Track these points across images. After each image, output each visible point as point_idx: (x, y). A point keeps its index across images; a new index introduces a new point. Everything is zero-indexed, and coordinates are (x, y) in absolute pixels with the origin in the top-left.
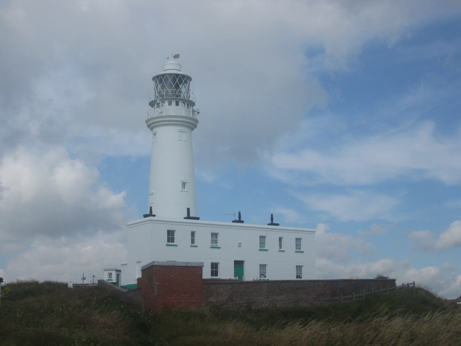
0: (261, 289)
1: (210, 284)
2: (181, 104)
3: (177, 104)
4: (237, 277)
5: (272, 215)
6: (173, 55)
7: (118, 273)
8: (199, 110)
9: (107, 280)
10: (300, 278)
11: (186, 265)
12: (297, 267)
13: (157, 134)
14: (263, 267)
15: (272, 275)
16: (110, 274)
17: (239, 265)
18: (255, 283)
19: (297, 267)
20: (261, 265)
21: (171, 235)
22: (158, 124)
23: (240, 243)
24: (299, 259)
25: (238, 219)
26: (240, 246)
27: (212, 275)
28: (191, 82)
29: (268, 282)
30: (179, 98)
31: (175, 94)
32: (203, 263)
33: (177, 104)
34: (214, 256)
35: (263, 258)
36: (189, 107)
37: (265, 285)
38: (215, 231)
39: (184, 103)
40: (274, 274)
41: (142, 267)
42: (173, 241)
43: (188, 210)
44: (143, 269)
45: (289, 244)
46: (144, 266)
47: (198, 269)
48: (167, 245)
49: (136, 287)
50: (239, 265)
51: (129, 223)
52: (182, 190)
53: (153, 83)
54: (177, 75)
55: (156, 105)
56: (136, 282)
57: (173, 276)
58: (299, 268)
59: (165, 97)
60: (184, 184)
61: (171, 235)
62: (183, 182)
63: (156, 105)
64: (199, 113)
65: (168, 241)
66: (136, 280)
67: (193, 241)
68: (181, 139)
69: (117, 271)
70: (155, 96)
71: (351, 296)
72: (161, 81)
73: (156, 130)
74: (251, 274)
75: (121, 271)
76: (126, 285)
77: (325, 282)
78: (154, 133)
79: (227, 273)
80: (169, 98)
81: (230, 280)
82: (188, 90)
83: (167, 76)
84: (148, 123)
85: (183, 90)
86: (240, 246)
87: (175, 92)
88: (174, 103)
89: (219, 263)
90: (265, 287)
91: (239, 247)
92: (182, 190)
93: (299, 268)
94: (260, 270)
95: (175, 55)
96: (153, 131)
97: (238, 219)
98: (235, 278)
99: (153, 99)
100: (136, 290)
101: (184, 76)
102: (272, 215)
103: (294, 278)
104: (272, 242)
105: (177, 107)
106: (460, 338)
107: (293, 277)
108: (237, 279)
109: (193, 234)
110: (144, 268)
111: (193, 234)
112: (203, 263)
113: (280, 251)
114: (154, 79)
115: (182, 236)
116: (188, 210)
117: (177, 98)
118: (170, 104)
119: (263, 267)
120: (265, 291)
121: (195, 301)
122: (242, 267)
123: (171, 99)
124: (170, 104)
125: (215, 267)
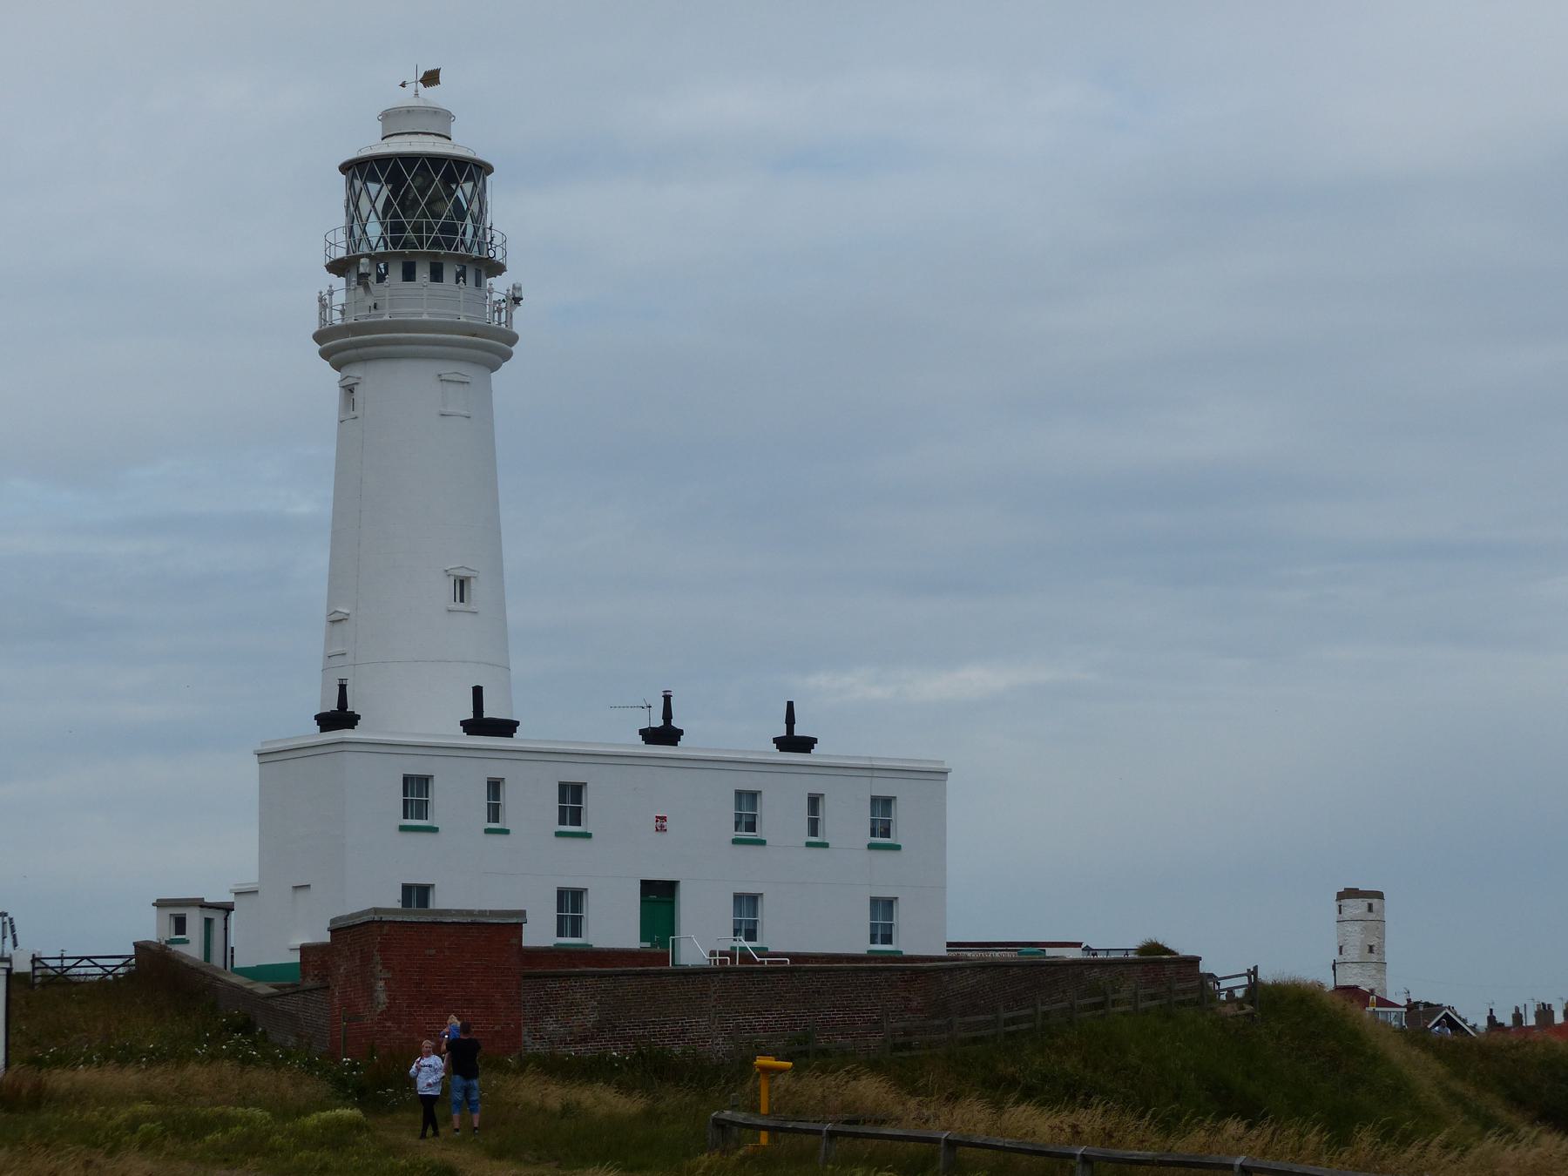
2: (449, 274)
3: (436, 275)
5: (790, 705)
6: (421, 76)
10: (887, 939)
13: (358, 390)
14: (747, 903)
15: (783, 934)
16: (180, 924)
17: (659, 898)
20: (738, 898)
21: (416, 790)
22: (360, 351)
23: (664, 819)
24: (884, 875)
27: (560, 933)
32: (522, 913)
33: (436, 275)
34: (572, 864)
35: (749, 870)
38: (748, 784)
41: (333, 921)
43: (478, 692)
45: (848, 819)
46: (340, 918)
47: (508, 928)
48: (403, 828)
50: (659, 898)
54: (436, 161)
58: (883, 907)
60: (462, 582)
61: (416, 790)
67: (494, 813)
68: (449, 410)
71: (989, 1017)
72: (396, 180)
73: (356, 371)
74: (701, 938)
78: (346, 383)
79: (614, 926)
87: (430, 229)
88: (423, 273)
92: (453, 606)
93: (883, 907)
99: (341, 253)
102: (790, 705)
103: (859, 944)
104: (781, 815)
107: (854, 940)
112: (522, 913)
113: (809, 845)
114: (345, 168)
116: (478, 692)
117: (436, 254)
118: (409, 275)
121: (497, 1028)
124: (409, 275)
125: (571, 902)
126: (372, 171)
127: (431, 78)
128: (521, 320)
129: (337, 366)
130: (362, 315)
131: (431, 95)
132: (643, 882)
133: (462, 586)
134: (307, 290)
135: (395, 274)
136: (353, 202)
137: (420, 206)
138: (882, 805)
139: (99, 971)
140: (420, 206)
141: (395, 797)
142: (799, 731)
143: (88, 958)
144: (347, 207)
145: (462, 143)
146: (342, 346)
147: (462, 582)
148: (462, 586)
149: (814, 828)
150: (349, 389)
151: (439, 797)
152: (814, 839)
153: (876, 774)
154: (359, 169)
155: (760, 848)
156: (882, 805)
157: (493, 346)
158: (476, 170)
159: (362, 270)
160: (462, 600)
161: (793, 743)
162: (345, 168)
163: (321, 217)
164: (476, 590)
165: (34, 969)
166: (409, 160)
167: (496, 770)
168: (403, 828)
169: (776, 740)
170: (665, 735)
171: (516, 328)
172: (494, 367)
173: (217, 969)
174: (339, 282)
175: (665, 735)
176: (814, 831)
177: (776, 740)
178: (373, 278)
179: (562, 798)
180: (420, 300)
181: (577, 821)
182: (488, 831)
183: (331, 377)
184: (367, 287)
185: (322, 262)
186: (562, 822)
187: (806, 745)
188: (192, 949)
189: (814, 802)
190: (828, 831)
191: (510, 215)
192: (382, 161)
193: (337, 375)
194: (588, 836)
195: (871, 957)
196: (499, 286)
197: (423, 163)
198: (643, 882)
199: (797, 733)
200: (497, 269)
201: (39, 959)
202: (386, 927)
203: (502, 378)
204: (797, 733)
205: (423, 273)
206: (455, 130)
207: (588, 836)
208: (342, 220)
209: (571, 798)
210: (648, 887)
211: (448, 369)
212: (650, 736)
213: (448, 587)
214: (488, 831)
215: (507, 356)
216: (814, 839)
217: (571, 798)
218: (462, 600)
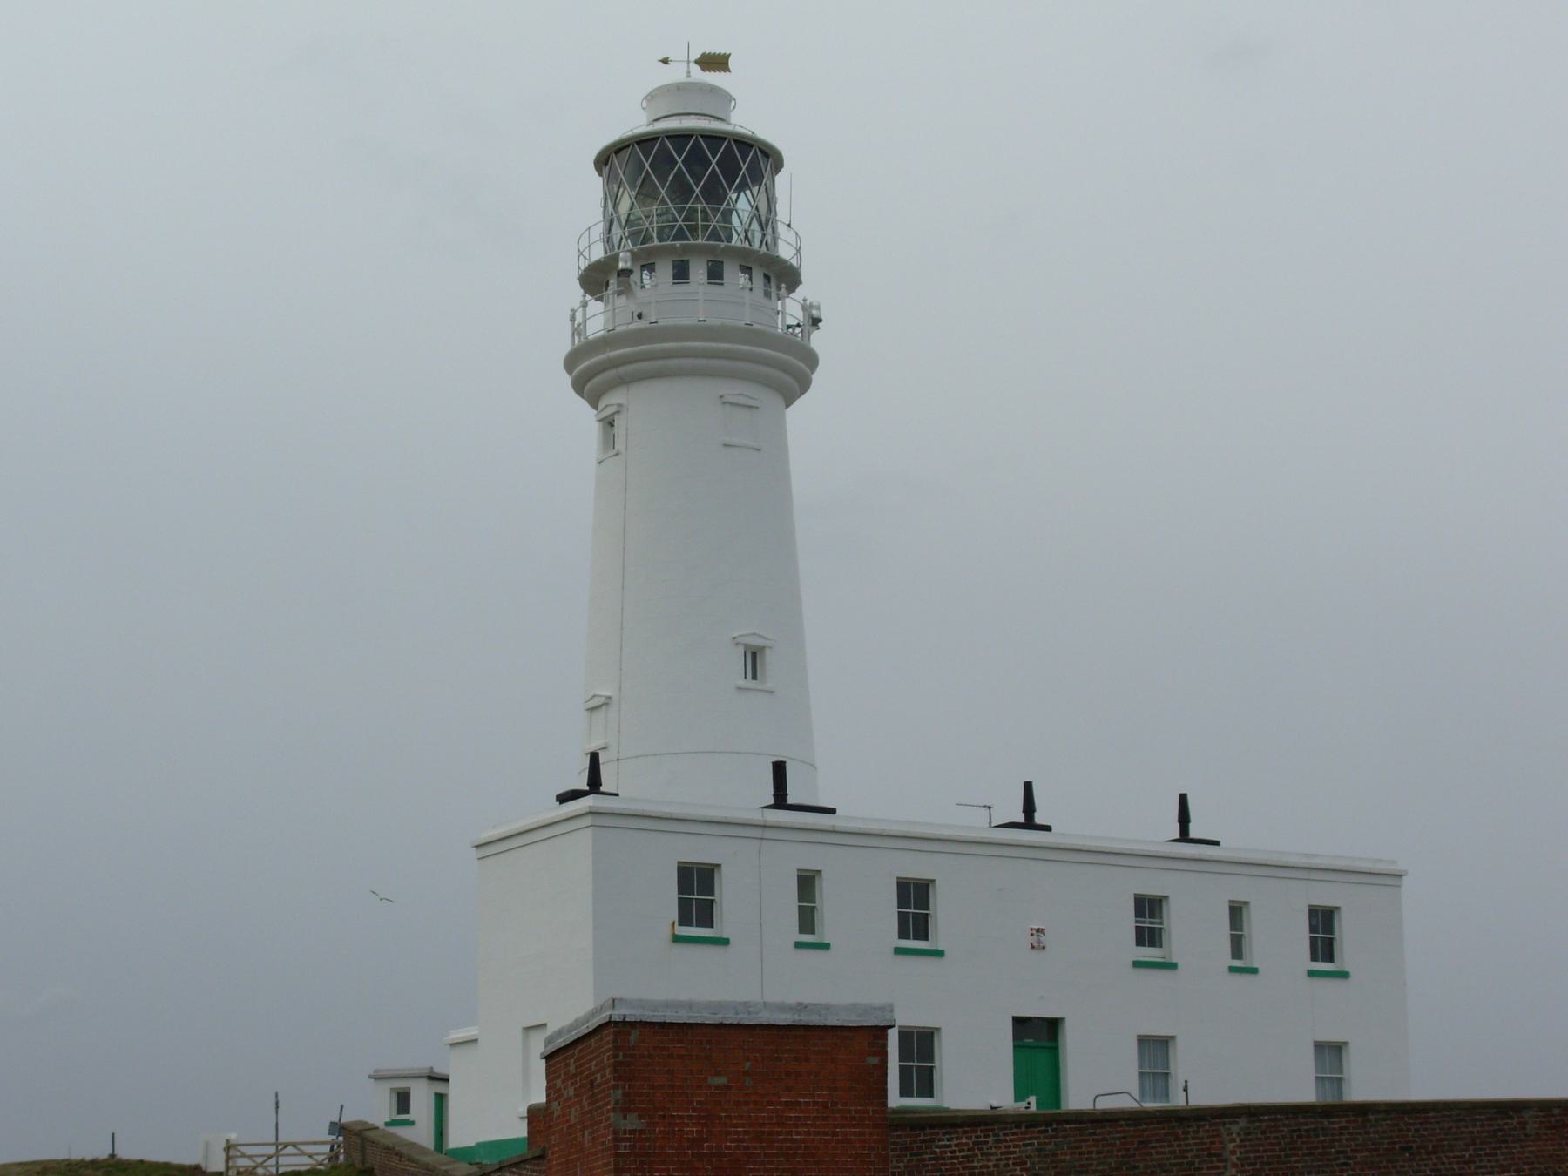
0: (1210, 1155)
1: (932, 1127)
3: (715, 275)
4: (1033, 1099)
6: (696, 55)
7: (439, 1088)
8: (818, 308)
9: (387, 1124)
11: (797, 1017)
13: (620, 422)
14: (1155, 1048)
17: (1038, 1038)
20: (1143, 1041)
21: (697, 892)
22: (622, 370)
24: (1329, 1011)
25: (1021, 818)
26: (1038, 946)
28: (781, 179)
30: (723, 245)
31: (706, 228)
33: (715, 275)
35: (1152, 1005)
36: (773, 290)
37: (1235, 1128)
39: (746, 269)
40: (1211, 1078)
42: (707, 921)
44: (552, 1048)
45: (1281, 937)
48: (899, 951)
49: (523, 1150)
50: (1038, 1038)
52: (742, 683)
55: (613, 281)
56: (521, 1130)
57: (722, 1080)
58: (1330, 1053)
59: (656, 242)
60: (754, 655)
61: (697, 892)
62: (746, 646)
63: (613, 281)
64: (820, 320)
65: (684, 919)
67: (807, 920)
69: (433, 1078)
70: (609, 240)
73: (612, 400)
74: (1098, 1079)
75: (447, 1080)
76: (472, 1143)
77: (1556, 1111)
78: (603, 415)
80: (678, 243)
82: (766, 221)
83: (663, 143)
84: (579, 369)
85: (743, 204)
86: (1038, 946)
88: (698, 271)
89: (938, 1029)
90: (1233, 1140)
91: (1034, 952)
92: (742, 683)
93: (1330, 1053)
94: (1141, 1066)
95: (704, 55)
96: (601, 407)
97: (1021, 818)
98: (1024, 1104)
99: (598, 253)
100: (516, 1164)
104: (1195, 926)
107: (1301, 1090)
108: (1033, 1108)
110: (561, 1042)
113: (1232, 969)
114: (604, 161)
115: (753, 896)
119: (1155, 1048)
120: (1235, 1165)
123: (685, 249)
124: (681, 273)
127: (715, 62)
128: (818, 341)
130: (626, 325)
131: (714, 78)
132: (1019, 1022)
133: (754, 658)
135: (665, 271)
137: (690, 182)
138: (1323, 921)
139: (309, 1161)
140: (690, 182)
141: (1129, 923)
143: (294, 1145)
144: (605, 207)
145: (744, 120)
147: (754, 655)
148: (754, 658)
149: (1237, 949)
150: (609, 423)
151: (729, 896)
152: (1237, 963)
156: (1323, 921)
157: (787, 368)
159: (621, 265)
160: (754, 677)
163: (577, 214)
164: (770, 661)
165: (228, 1168)
166: (680, 138)
167: (809, 859)
173: (422, 1150)
176: (1237, 952)
180: (695, 303)
181: (923, 934)
182: (799, 945)
183: (584, 417)
186: (903, 934)
188: (420, 1132)
189: (1237, 912)
191: (807, 210)
194: (939, 954)
196: (792, 309)
197: (697, 145)
198: (1019, 1022)
201: (235, 1146)
202: (634, 1036)
205: (698, 271)
207: (939, 954)
209: (914, 905)
210: (1022, 1025)
211: (732, 390)
213: (737, 660)
214: (799, 945)
216: (1237, 963)
217: (914, 905)
218: (754, 677)
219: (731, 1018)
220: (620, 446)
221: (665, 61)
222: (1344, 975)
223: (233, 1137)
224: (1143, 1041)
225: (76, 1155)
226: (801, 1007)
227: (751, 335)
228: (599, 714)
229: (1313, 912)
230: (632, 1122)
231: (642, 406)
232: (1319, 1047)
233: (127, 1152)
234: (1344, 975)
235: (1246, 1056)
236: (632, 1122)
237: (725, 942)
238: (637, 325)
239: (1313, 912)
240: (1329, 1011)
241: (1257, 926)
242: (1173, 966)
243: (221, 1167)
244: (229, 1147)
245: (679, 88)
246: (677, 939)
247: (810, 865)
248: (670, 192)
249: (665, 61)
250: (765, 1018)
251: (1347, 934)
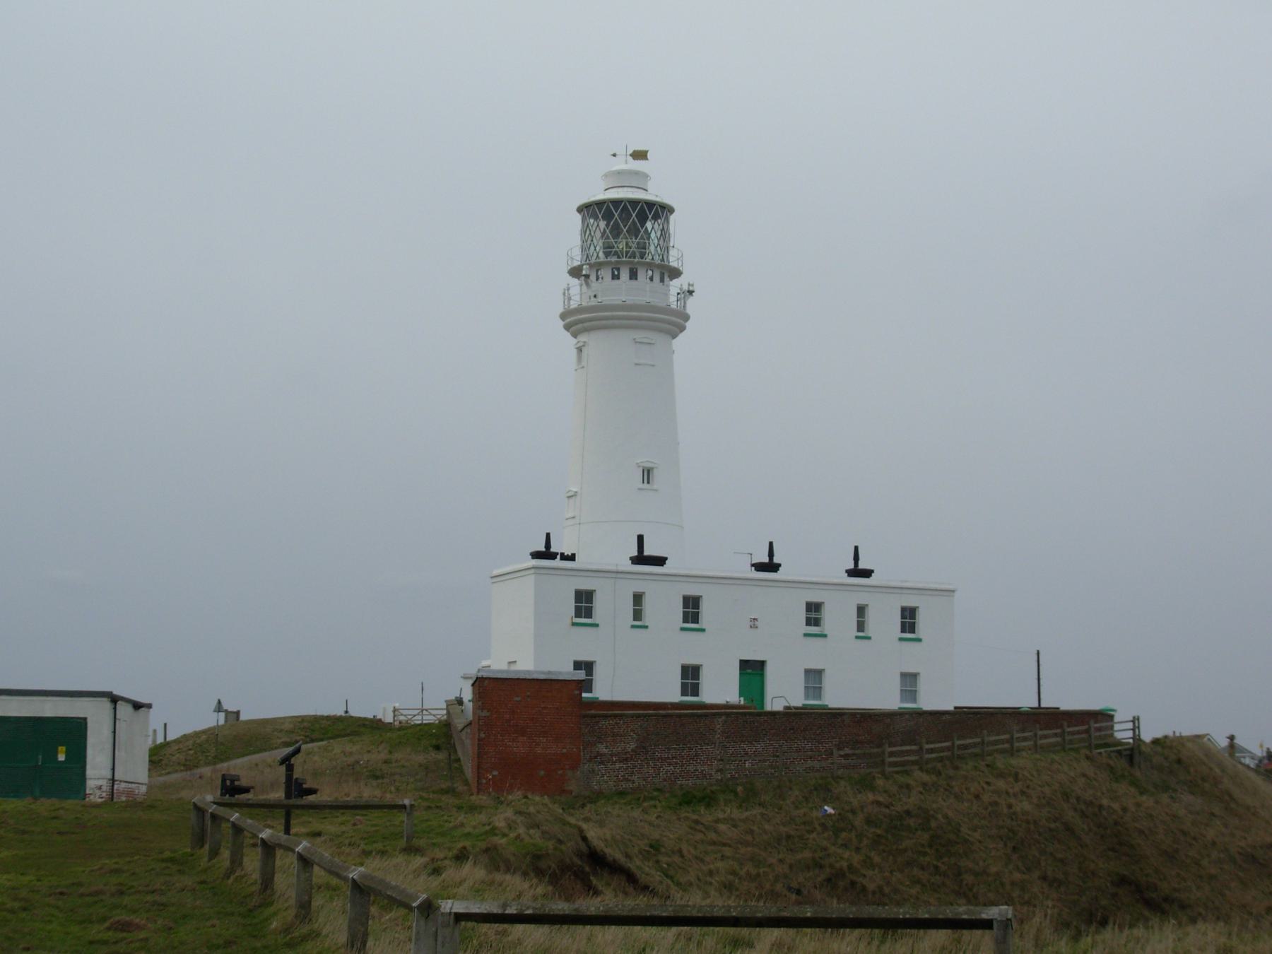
3: (633, 275)
6: (630, 151)
12: (904, 676)
14: (814, 677)
15: (837, 696)
17: (752, 670)
18: (792, 716)
19: (904, 676)
20: (808, 672)
21: (814, 612)
22: (586, 325)
24: (911, 657)
26: (754, 627)
27: (684, 693)
28: (672, 218)
29: (921, 714)
33: (633, 275)
34: (692, 649)
38: (814, 598)
43: (640, 539)
45: (885, 621)
48: (683, 629)
50: (752, 670)
51: (496, 572)
52: (641, 486)
53: (579, 217)
54: (634, 203)
58: (909, 681)
61: (814, 612)
65: (578, 615)
66: (219, 708)
67: (861, 626)
72: (608, 216)
73: (583, 338)
74: (783, 692)
79: (721, 688)
81: (728, 706)
86: (754, 627)
88: (625, 274)
93: (909, 681)
99: (576, 263)
101: (651, 205)
104: (838, 617)
105: (633, 282)
106: (5, 853)
107: (670, 692)
109: (861, 610)
111: (861, 610)
114: (580, 210)
116: (640, 539)
119: (814, 677)
122: (762, 675)
126: (594, 210)
127: (640, 155)
128: (692, 305)
129: (575, 335)
131: (638, 165)
133: (647, 474)
134: (555, 288)
135: (606, 274)
136: (585, 229)
141: (802, 615)
142: (862, 566)
146: (578, 322)
148: (647, 474)
150: (580, 350)
151: (827, 615)
153: (543, 571)
154: (589, 210)
155: (866, 641)
158: (659, 211)
161: (857, 572)
162: (580, 210)
163: (567, 238)
166: (616, 203)
167: (863, 599)
168: (633, 627)
169: (847, 571)
170: (770, 566)
171: (689, 310)
172: (674, 337)
174: (575, 282)
175: (770, 566)
177: (847, 571)
178: (593, 277)
179: (903, 617)
180: (621, 291)
182: (633, 627)
183: (569, 341)
184: (587, 284)
185: (566, 269)
186: (903, 631)
187: (867, 573)
190: (871, 628)
191: (685, 239)
192: (600, 204)
193: (575, 341)
195: (805, 707)
196: (675, 285)
199: (646, 553)
200: (675, 273)
203: (679, 342)
204: (646, 553)
206: (651, 186)
208: (578, 242)
209: (909, 619)
210: (745, 665)
211: (640, 335)
212: (760, 567)
215: (682, 329)
217: (909, 619)
219: (522, 676)
220: (584, 363)
221: (614, 155)
222: (919, 640)
223: (397, 705)
224: (808, 672)
225: (319, 713)
226: (549, 672)
227: (649, 308)
228: (571, 501)
229: (903, 609)
230: (485, 713)
231: (596, 342)
232: (904, 675)
233: (355, 712)
234: (919, 640)
235: (862, 680)
236: (485, 713)
237: (597, 625)
238: (594, 302)
239: (903, 609)
240: (911, 657)
241: (871, 617)
242: (825, 636)
243: (391, 720)
244: (395, 710)
245: (619, 173)
246: (574, 624)
247: (640, 590)
248: (620, 216)
249: (614, 155)
250: (535, 676)
251: (922, 620)
